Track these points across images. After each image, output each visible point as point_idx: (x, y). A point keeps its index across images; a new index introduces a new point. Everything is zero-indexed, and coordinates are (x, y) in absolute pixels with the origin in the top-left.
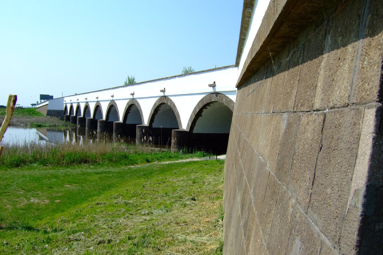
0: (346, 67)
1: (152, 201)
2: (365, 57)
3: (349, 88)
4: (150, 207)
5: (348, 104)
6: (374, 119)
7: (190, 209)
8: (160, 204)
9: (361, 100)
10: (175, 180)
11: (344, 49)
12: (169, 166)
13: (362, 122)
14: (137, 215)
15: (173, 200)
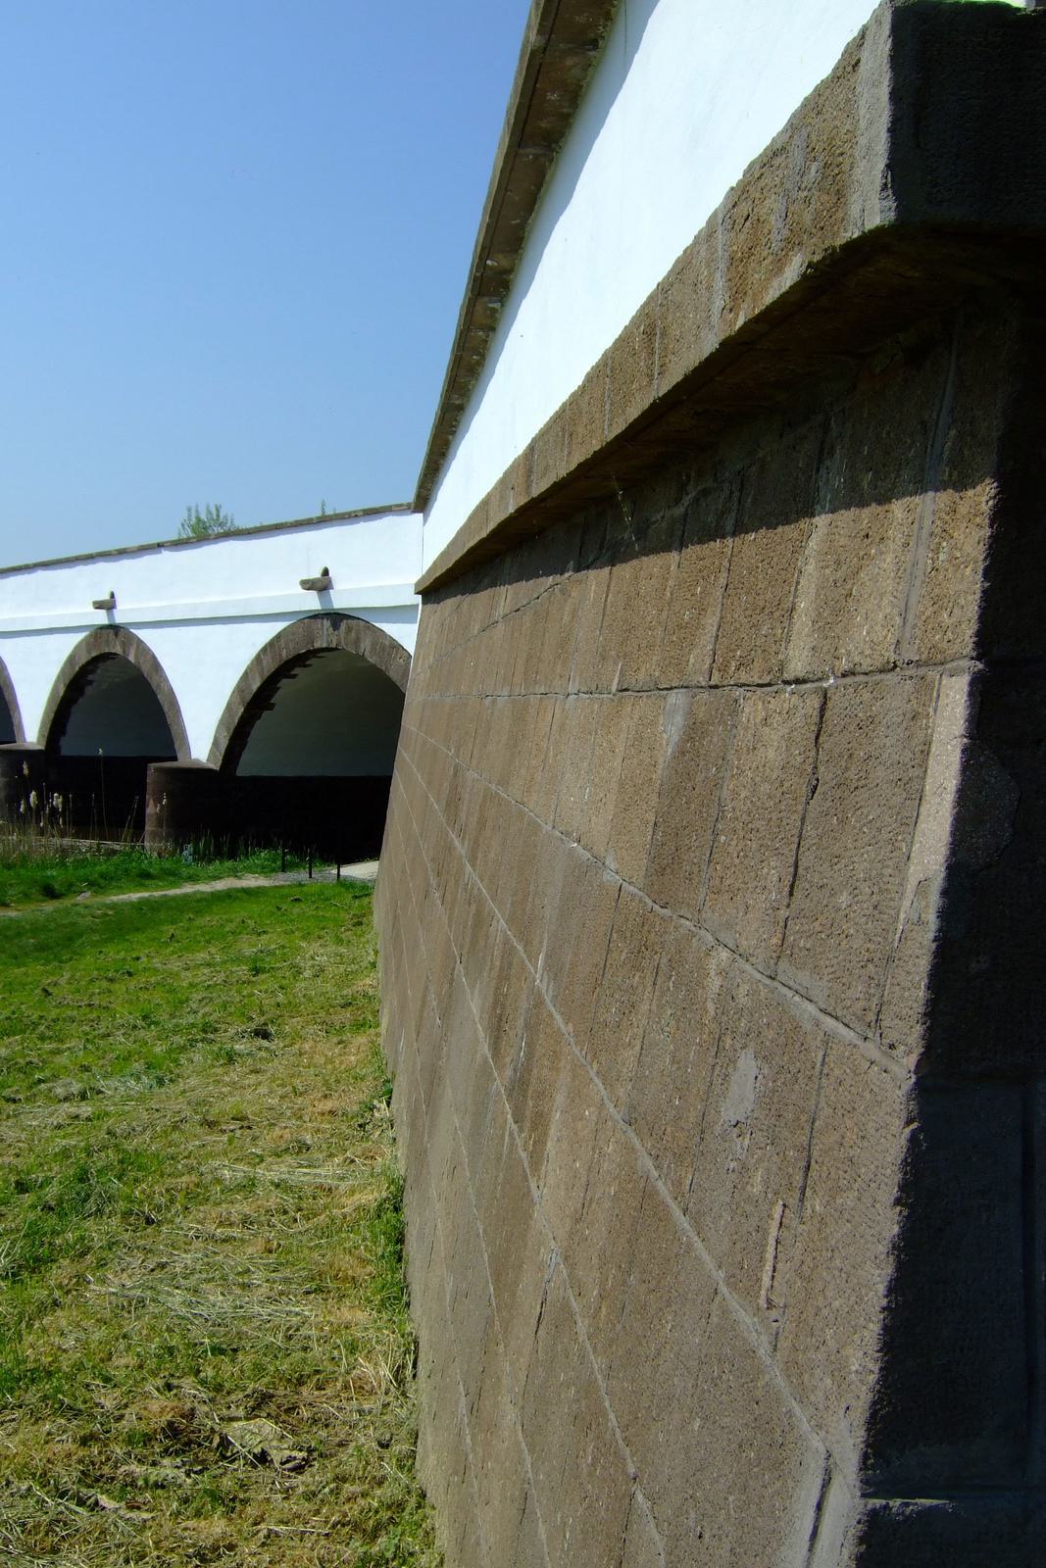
0: (888, 560)
1: (90, 1046)
2: (941, 540)
3: (898, 620)
4: (86, 1069)
5: (894, 663)
6: (966, 701)
7: (252, 1072)
8: (127, 1058)
9: (931, 655)
10: (175, 965)
11: (880, 508)
12: (142, 909)
13: (935, 711)
14: (35, 1102)
15: (179, 1040)
